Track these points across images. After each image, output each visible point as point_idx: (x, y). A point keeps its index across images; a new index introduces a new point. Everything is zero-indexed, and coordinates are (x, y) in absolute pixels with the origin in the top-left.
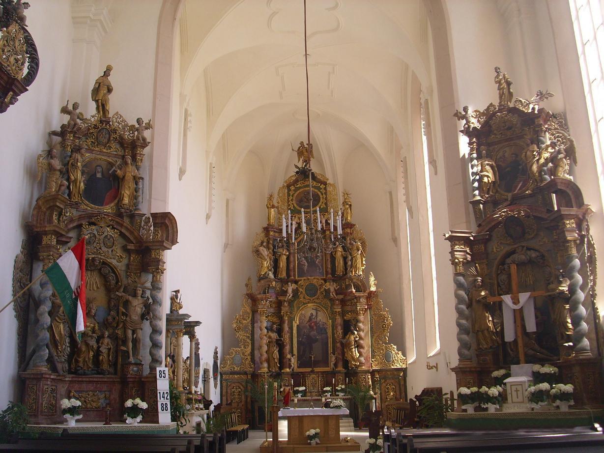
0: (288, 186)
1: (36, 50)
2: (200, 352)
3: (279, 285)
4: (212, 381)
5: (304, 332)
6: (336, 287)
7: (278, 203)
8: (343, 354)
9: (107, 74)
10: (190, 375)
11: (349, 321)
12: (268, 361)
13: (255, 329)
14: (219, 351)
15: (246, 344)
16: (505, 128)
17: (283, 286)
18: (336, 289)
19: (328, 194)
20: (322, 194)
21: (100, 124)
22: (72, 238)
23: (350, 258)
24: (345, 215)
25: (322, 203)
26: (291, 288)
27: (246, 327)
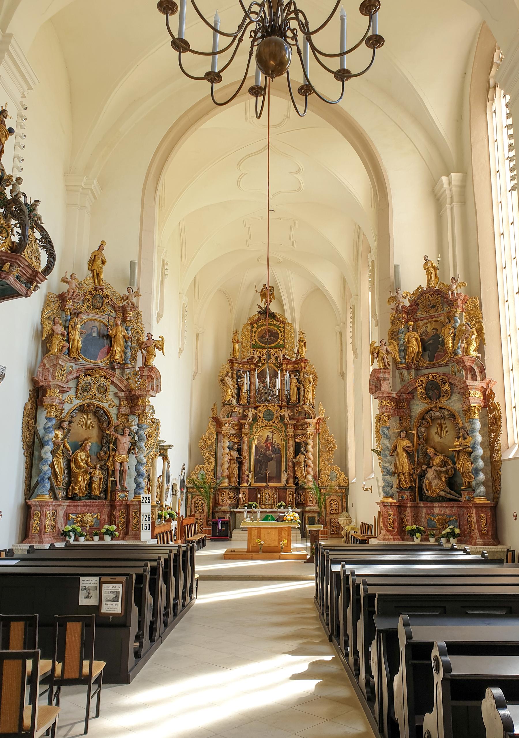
0: (252, 324)
1: (53, 248)
2: (170, 469)
3: (241, 410)
4: (179, 495)
5: (261, 451)
6: (290, 413)
7: (242, 338)
8: (294, 471)
9: (101, 248)
10: (161, 492)
11: (300, 443)
12: (229, 476)
13: (218, 448)
14: (186, 467)
15: (210, 461)
16: (430, 306)
17: (244, 411)
18: (290, 415)
19: (286, 332)
20: (281, 332)
21: (95, 291)
22: (72, 388)
23: (303, 389)
24: (300, 351)
25: (281, 339)
26: (251, 413)
27: (211, 446)
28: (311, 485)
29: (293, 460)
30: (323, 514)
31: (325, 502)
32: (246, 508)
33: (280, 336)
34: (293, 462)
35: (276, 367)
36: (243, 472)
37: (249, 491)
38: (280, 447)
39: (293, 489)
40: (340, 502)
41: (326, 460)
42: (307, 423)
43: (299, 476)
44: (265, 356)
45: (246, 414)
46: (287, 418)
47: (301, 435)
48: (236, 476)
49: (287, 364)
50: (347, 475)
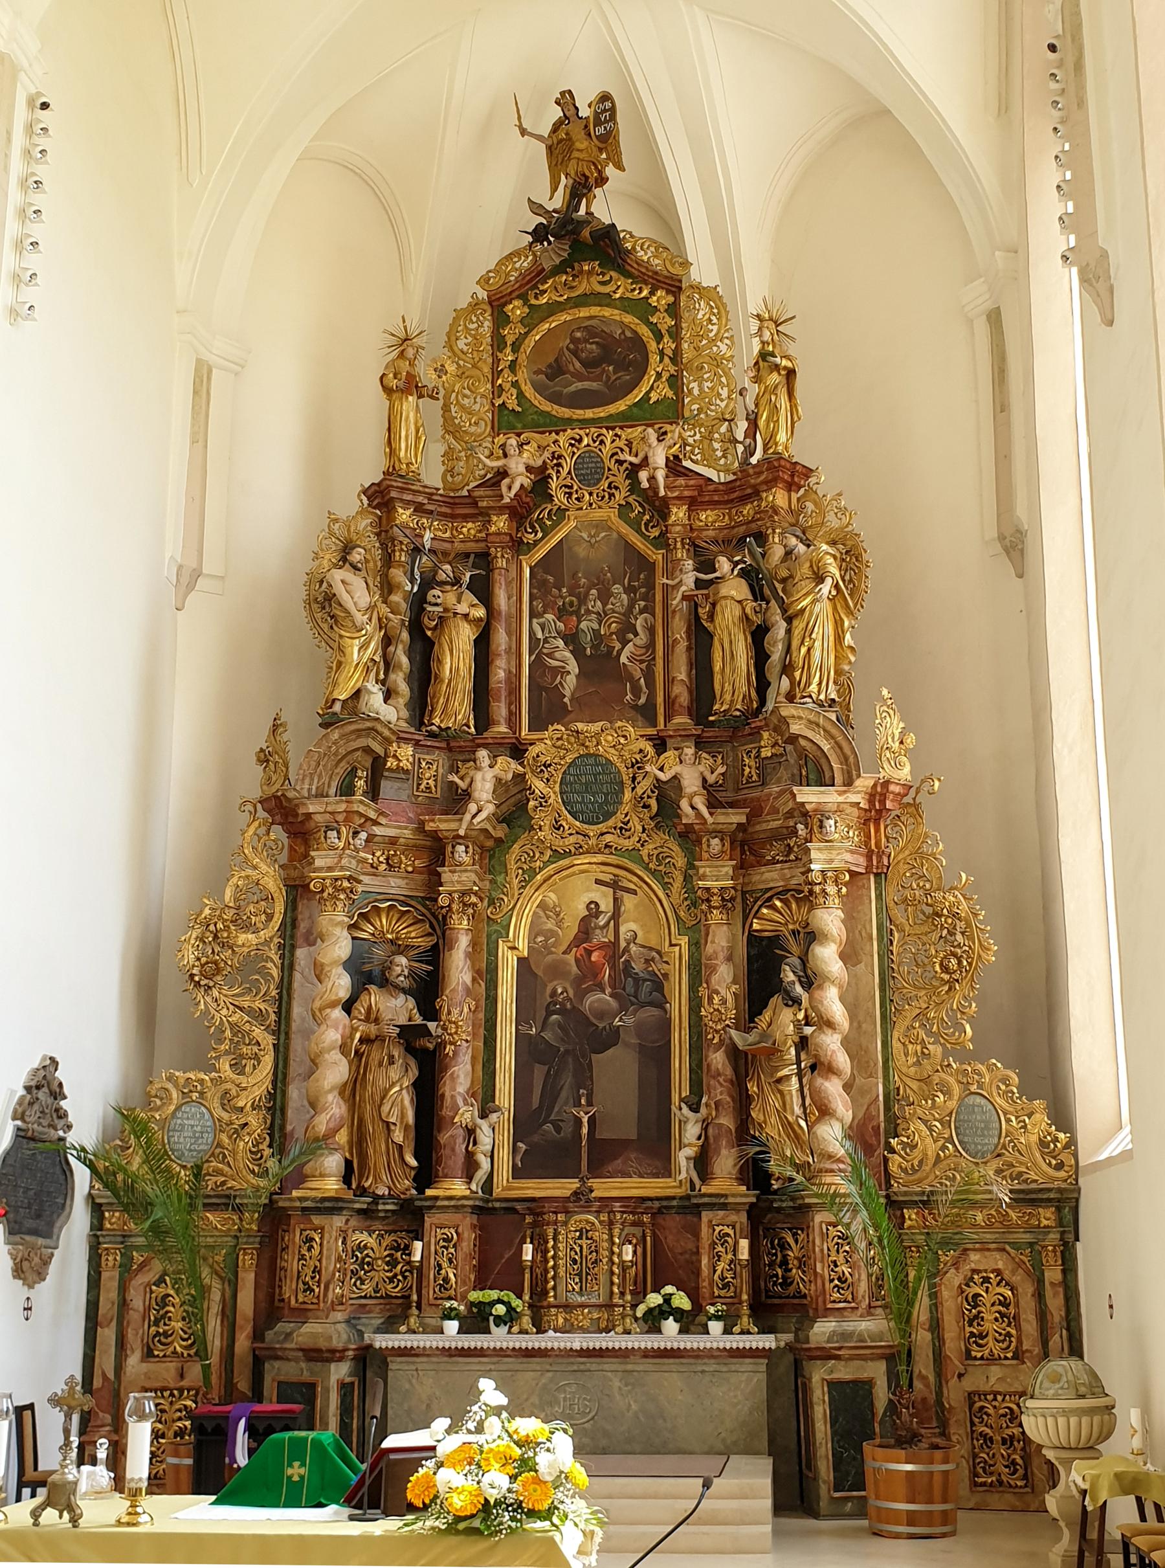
0: (497, 304)
5: (554, 993)
8: (743, 1103)
13: (297, 976)
19: (686, 334)
20: (659, 337)
23: (780, 629)
24: (762, 423)
27: (253, 962)
28: (840, 1183)
29: (733, 1032)
30: (924, 1365)
31: (932, 1286)
32: (452, 1326)
33: (654, 358)
34: (736, 1055)
35: (635, 525)
36: (446, 1112)
37: (482, 1229)
38: (658, 968)
39: (736, 1208)
40: (1027, 1290)
41: (930, 1033)
42: (805, 814)
43: (773, 1130)
44: (568, 465)
45: (463, 785)
46: (691, 798)
47: (781, 894)
48: (398, 1136)
49: (694, 504)
50: (1062, 1117)
